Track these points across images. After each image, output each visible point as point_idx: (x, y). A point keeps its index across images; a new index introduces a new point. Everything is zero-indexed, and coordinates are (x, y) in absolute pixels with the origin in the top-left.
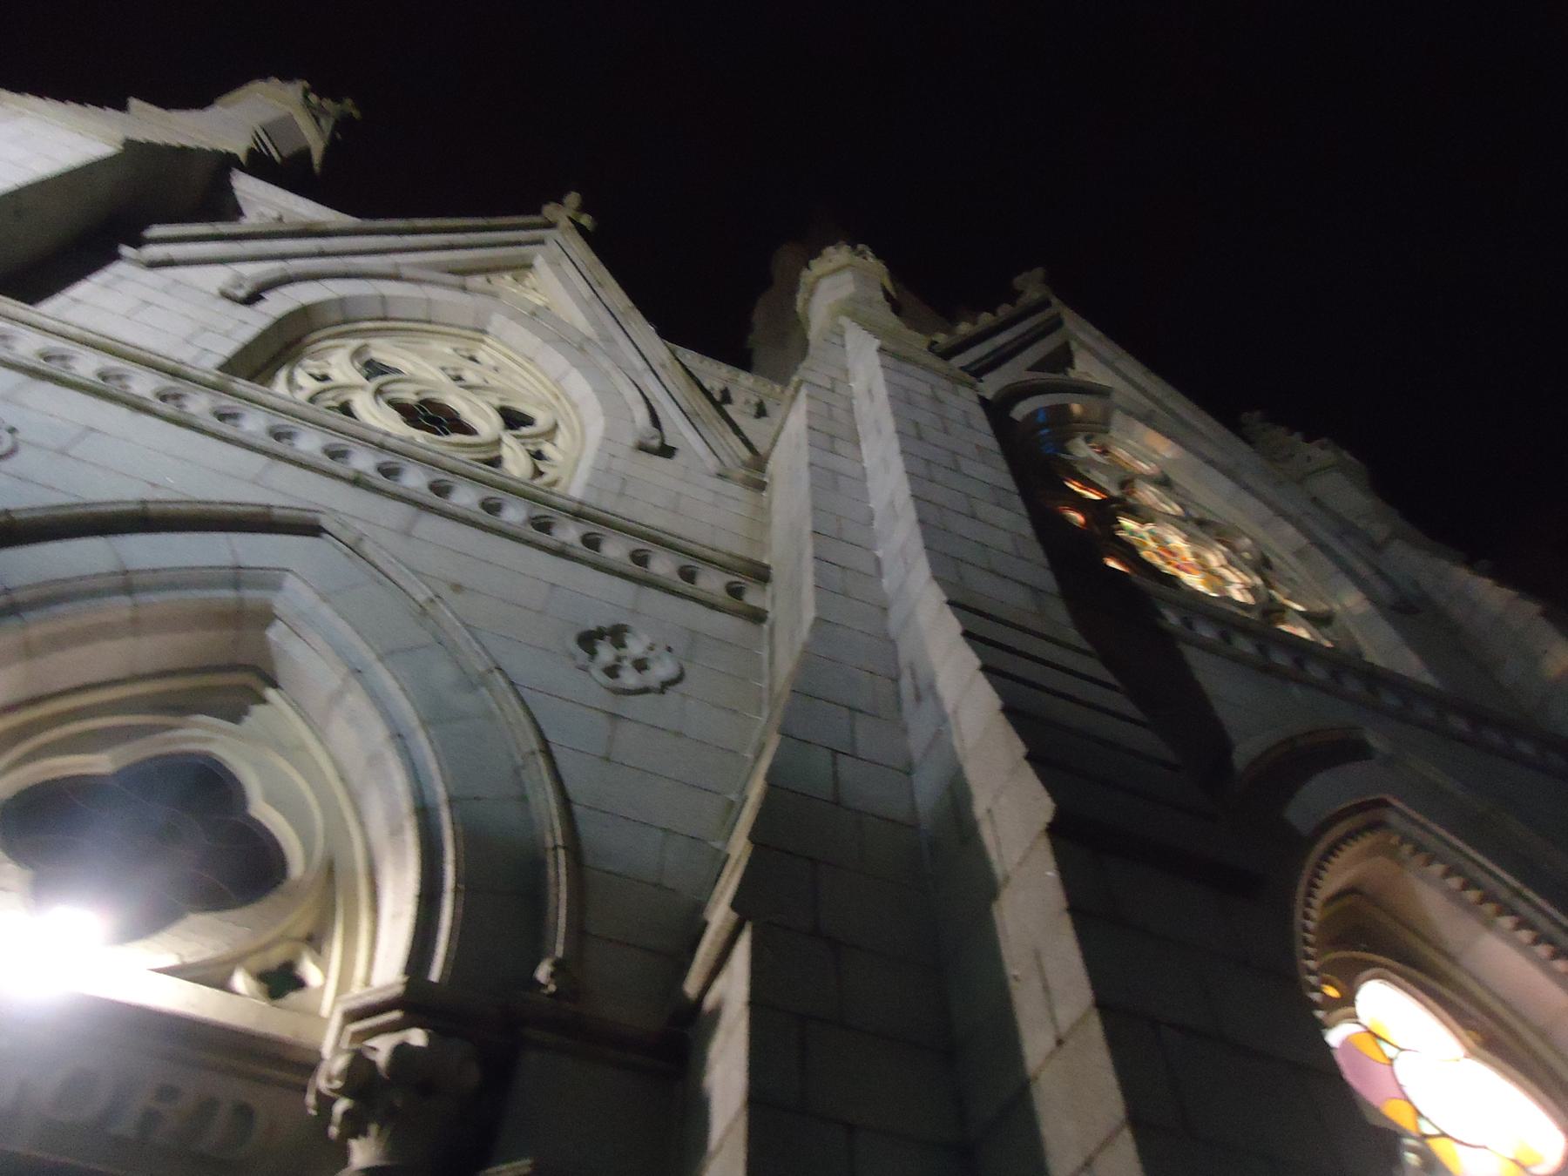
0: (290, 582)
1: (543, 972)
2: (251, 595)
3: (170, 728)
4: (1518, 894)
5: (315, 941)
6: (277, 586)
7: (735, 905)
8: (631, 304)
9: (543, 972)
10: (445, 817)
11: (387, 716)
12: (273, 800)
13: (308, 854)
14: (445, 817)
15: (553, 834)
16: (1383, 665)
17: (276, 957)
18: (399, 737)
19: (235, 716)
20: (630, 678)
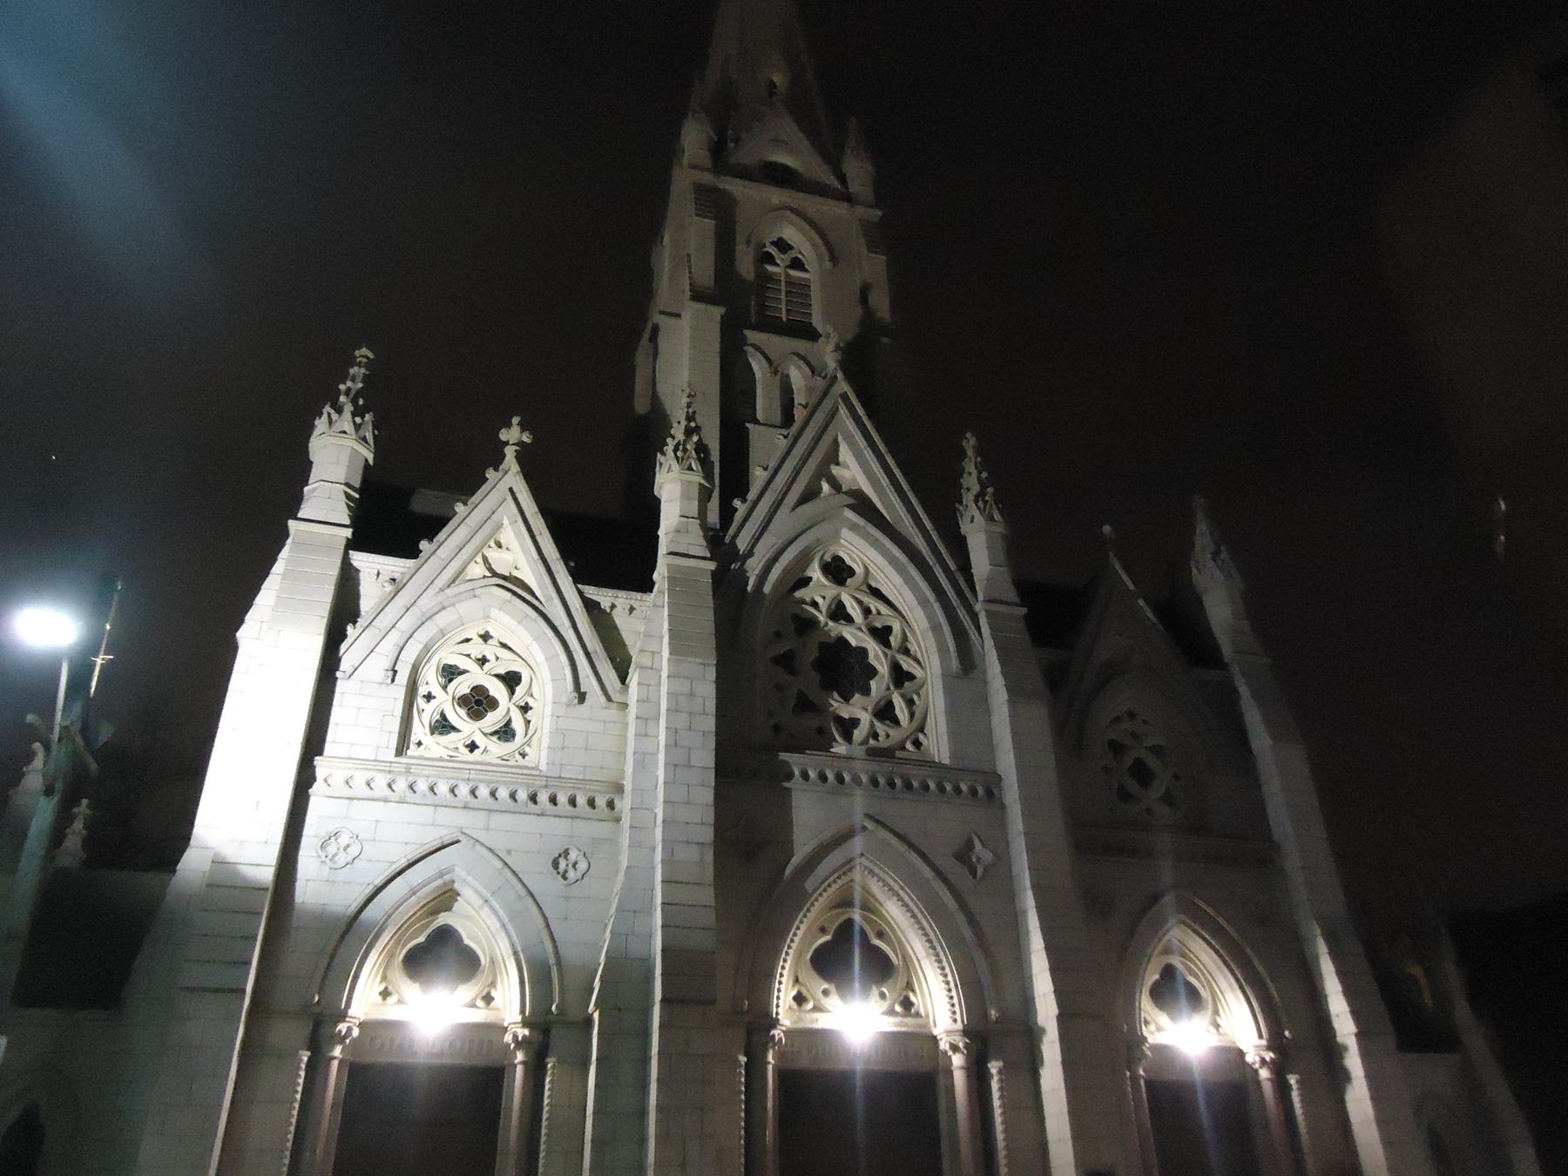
0: (457, 869)
1: (554, 1008)
2: (447, 878)
3: (434, 920)
4: (902, 889)
5: (493, 984)
6: (453, 871)
7: (595, 1005)
8: (559, 557)
9: (554, 1008)
10: (521, 954)
11: (500, 919)
12: (471, 939)
13: (485, 954)
14: (521, 954)
15: (552, 961)
16: (995, 651)
17: (484, 993)
18: (503, 926)
19: (449, 909)
20: (571, 874)
